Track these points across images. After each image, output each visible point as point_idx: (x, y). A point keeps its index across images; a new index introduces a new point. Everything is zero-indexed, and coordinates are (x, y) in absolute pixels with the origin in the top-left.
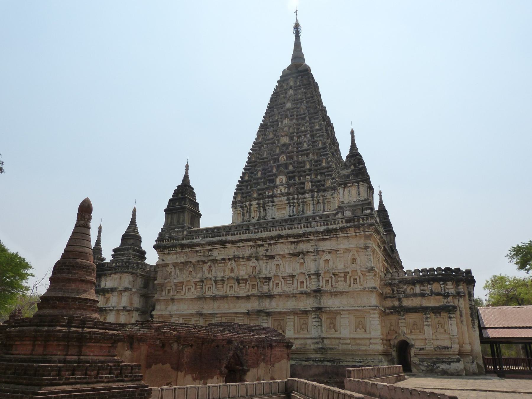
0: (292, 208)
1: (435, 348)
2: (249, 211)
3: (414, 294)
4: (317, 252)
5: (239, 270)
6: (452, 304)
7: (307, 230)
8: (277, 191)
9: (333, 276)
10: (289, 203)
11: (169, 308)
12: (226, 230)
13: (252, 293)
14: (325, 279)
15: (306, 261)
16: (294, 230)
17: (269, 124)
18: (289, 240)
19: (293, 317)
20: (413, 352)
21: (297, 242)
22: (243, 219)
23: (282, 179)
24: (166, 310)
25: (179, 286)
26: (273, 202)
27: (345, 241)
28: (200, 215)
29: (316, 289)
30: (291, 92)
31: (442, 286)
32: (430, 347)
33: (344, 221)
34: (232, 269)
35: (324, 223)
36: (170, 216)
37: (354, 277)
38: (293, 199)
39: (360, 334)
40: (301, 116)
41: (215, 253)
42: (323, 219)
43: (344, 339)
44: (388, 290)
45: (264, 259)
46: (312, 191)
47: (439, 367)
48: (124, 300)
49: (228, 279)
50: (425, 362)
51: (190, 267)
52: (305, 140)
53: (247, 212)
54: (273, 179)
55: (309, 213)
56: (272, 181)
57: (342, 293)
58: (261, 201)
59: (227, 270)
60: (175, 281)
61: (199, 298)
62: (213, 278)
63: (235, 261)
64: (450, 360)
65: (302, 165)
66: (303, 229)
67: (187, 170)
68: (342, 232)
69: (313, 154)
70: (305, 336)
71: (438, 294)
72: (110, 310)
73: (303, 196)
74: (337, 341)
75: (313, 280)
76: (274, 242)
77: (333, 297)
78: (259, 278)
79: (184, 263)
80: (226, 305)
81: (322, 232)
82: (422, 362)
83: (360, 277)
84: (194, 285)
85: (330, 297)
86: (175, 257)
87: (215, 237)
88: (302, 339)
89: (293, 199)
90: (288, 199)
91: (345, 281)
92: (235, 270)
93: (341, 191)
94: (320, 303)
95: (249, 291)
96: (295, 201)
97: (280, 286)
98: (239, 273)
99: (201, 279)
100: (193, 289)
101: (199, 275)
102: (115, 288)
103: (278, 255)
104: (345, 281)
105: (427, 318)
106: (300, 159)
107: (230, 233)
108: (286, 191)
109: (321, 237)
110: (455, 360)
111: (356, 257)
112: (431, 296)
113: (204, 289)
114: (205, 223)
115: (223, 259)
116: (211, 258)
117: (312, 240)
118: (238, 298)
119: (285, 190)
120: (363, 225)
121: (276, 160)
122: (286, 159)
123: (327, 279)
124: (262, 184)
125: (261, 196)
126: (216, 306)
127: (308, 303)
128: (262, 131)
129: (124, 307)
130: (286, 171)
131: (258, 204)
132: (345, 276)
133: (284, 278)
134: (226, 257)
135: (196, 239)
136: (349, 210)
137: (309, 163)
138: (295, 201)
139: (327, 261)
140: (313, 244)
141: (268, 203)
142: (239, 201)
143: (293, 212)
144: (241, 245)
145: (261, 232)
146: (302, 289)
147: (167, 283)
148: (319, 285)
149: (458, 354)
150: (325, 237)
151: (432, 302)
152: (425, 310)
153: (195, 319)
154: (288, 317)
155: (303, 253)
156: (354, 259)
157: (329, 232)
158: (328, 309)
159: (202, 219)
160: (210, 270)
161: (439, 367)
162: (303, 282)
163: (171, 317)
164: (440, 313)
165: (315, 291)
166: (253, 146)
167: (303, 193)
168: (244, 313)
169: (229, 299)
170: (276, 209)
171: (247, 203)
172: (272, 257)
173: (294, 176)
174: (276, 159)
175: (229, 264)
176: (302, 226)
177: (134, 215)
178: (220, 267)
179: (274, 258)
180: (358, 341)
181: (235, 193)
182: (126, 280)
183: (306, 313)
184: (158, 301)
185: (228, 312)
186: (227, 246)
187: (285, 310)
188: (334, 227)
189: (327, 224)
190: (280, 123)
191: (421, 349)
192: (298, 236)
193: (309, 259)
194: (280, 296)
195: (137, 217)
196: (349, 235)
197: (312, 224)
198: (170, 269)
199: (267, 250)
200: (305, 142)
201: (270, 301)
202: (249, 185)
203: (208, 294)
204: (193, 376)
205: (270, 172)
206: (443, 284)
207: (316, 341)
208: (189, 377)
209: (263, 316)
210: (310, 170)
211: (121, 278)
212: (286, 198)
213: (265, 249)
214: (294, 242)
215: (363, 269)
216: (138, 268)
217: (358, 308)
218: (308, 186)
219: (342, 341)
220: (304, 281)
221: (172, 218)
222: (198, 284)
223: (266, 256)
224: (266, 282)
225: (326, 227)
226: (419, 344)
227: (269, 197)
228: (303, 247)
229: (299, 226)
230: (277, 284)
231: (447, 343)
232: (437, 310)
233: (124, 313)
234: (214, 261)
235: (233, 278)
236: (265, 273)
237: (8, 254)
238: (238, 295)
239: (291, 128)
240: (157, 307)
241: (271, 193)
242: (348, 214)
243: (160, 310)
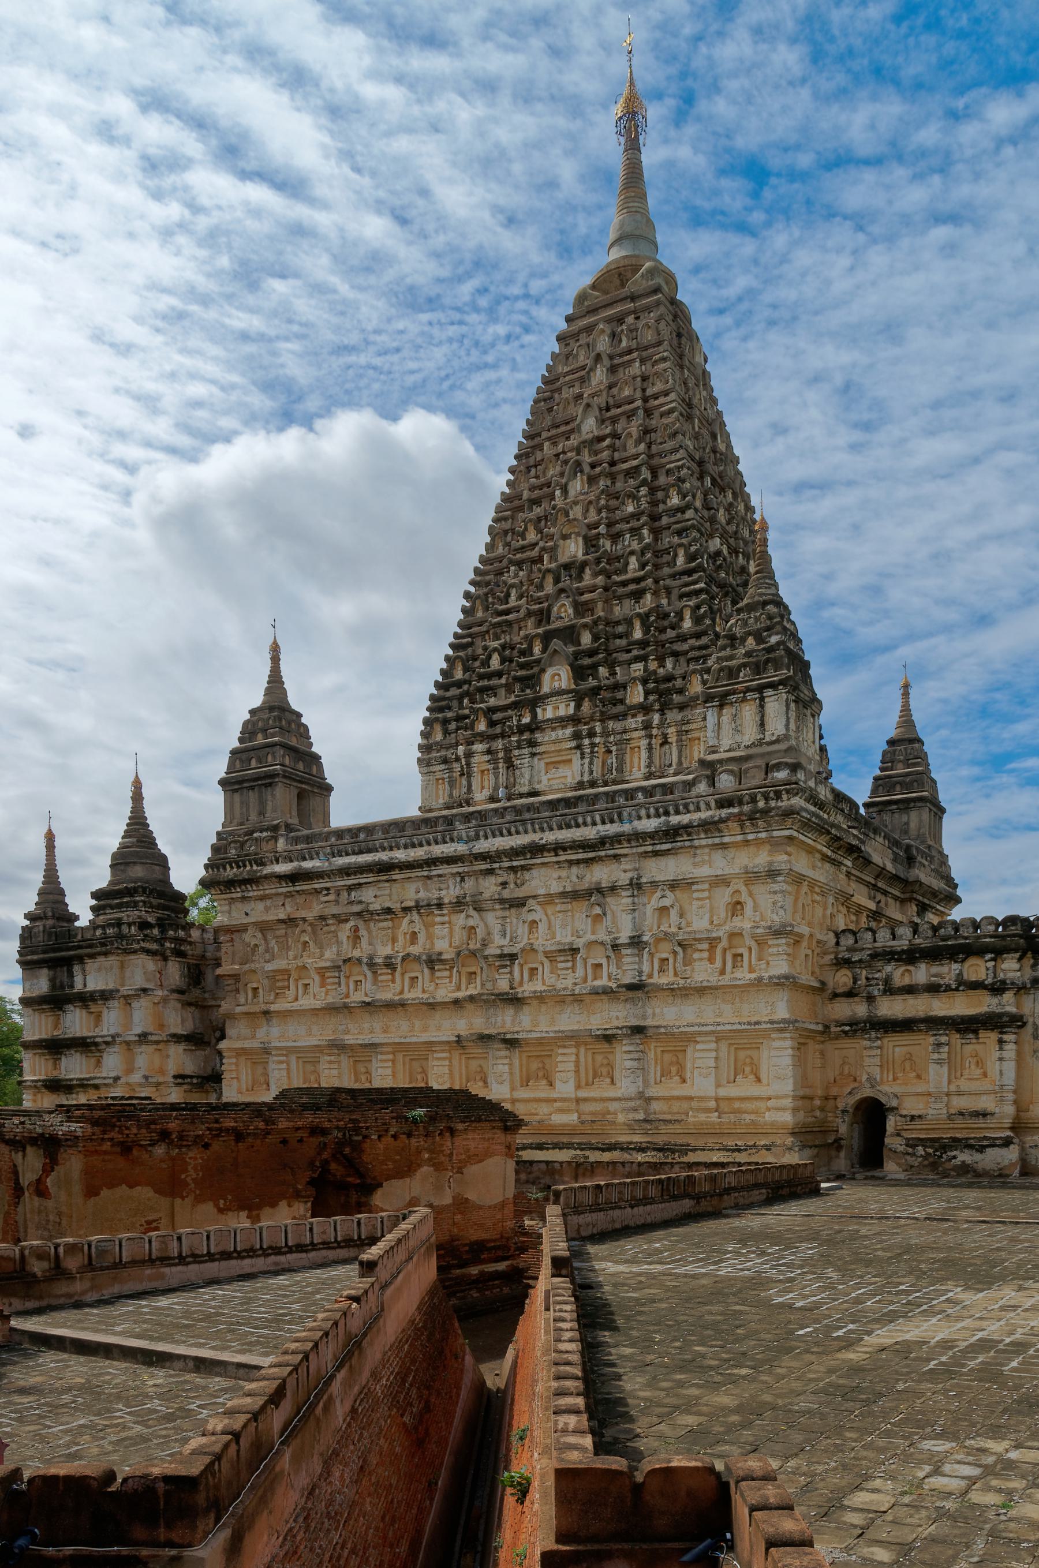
0: (587, 761)
1: (950, 1117)
2: (467, 773)
3: (910, 986)
4: (636, 885)
5: (430, 937)
6: (1012, 1009)
7: (611, 829)
8: (547, 712)
9: (679, 949)
10: (579, 747)
11: (261, 1033)
12: (396, 830)
13: (468, 993)
14: (658, 956)
15: (609, 912)
16: (574, 830)
17: (526, 495)
18: (562, 858)
19: (574, 1050)
20: (891, 1123)
21: (588, 862)
22: (451, 796)
23: (558, 677)
24: (254, 1037)
25: (279, 980)
26: (532, 743)
27: (717, 856)
28: (329, 789)
29: (633, 981)
30: (600, 376)
31: (991, 964)
32: (935, 1111)
33: (713, 804)
34: (414, 934)
35: (657, 810)
36: (237, 797)
37: (734, 951)
38: (591, 734)
39: (744, 1088)
40: (625, 466)
41: (367, 895)
42: (656, 799)
43: (701, 1099)
44: (843, 979)
45: (497, 907)
46: (645, 708)
47: (955, 1157)
48: (141, 1017)
49: (403, 959)
50: (920, 1148)
51: (304, 931)
52: (635, 546)
53: (462, 775)
54: (532, 676)
55: (636, 775)
56: (532, 681)
57: (701, 991)
58: (499, 744)
59: (401, 938)
60: (269, 967)
61: (332, 1009)
62: (365, 960)
63: (419, 913)
64: (985, 1143)
65: (620, 629)
66: (600, 827)
67: (275, 660)
68: (706, 832)
69: (656, 593)
70: (605, 1095)
71: (976, 985)
72: (107, 1043)
74: (685, 1105)
76: (522, 863)
78: (486, 957)
79: (290, 922)
80: (404, 1025)
81: (652, 835)
82: (914, 1146)
83: (750, 949)
84: (317, 978)
85: (670, 1000)
86: (260, 906)
87: (361, 852)
88: (595, 1100)
89: (591, 734)
90: (577, 736)
91: (711, 960)
92: (421, 937)
93: (711, 717)
94: (644, 1017)
95: (459, 989)
96: (597, 740)
97: (540, 977)
98: (433, 944)
99: (332, 961)
100: (315, 987)
101: (330, 954)
102: (111, 991)
103: (534, 897)
104: (711, 960)
105: (939, 1045)
106: (617, 610)
107: (403, 841)
108: (571, 711)
109: (650, 848)
110: (998, 1142)
111: (744, 897)
113: (343, 987)
114: (343, 812)
115: (388, 911)
117: (625, 855)
118: (432, 1006)
119: (566, 708)
120: (765, 812)
121: (543, 616)
122: (571, 611)
123: (664, 955)
124: (502, 692)
125: (498, 730)
126: (377, 1026)
127: (615, 1015)
128: (505, 519)
129: (139, 1036)
130: (571, 649)
131: (489, 752)
132: (712, 949)
133: (548, 955)
134: (396, 906)
135: (312, 858)
136: (731, 772)
137: (643, 624)
138: (597, 740)
139: (664, 910)
140: (628, 867)
141: (519, 748)
142: (437, 743)
143: (591, 772)
144: (434, 873)
145: (486, 838)
146: (598, 983)
147: (245, 973)
148: (640, 973)
149: (1012, 1129)
151: (961, 1006)
152: (934, 1023)
153: (328, 1058)
154: (560, 1051)
155: (599, 890)
156: (739, 903)
157: (671, 833)
158: (663, 1030)
159: (335, 800)
160: (356, 938)
161: (955, 1157)
162: (600, 965)
163: (269, 1053)
164: (976, 1032)
165: (632, 987)
166: (476, 571)
167: (623, 716)
168: (448, 1042)
169: (411, 1009)
170: (542, 764)
171: (461, 750)
172: (518, 903)
173: (594, 667)
174: (541, 611)
175: (406, 921)
176: (598, 818)
177: (137, 797)
178: (384, 929)
180: (737, 1105)
181: (426, 722)
182: (140, 970)
183: (608, 1038)
184: (230, 1016)
185: (408, 1040)
186: (396, 875)
187: (552, 1035)
188: (685, 819)
189: (667, 813)
190: (558, 493)
191: (913, 1118)
193: (619, 904)
194: (540, 998)
195: (146, 803)
196: (726, 840)
197: (625, 814)
198: (251, 937)
199: (504, 884)
200: (632, 553)
201: (516, 1013)
202: (467, 694)
203: (357, 997)
204: (217, 1206)
205: (523, 653)
206: (992, 959)
207: (632, 1104)
208: (209, 1207)
209: (499, 1049)
210: (643, 644)
211: (122, 966)
212: (569, 731)
213: (500, 880)
214: (578, 862)
215: (760, 931)
216: (165, 939)
217: (739, 1027)
218: (636, 695)
219: (694, 1104)
220: (604, 961)
221: (245, 804)
222: (327, 975)
223: (502, 901)
224: (505, 966)
225: (663, 818)
226: (911, 1106)
227: (522, 729)
228: (601, 874)
229: (589, 819)
230: (533, 971)
231: (986, 1103)
232: (968, 1026)
234: (366, 915)
235: (417, 959)
236: (498, 944)
238: (431, 1000)
239: (592, 510)
240: (230, 1032)
241: (526, 720)
242: (726, 782)
243: (238, 1038)
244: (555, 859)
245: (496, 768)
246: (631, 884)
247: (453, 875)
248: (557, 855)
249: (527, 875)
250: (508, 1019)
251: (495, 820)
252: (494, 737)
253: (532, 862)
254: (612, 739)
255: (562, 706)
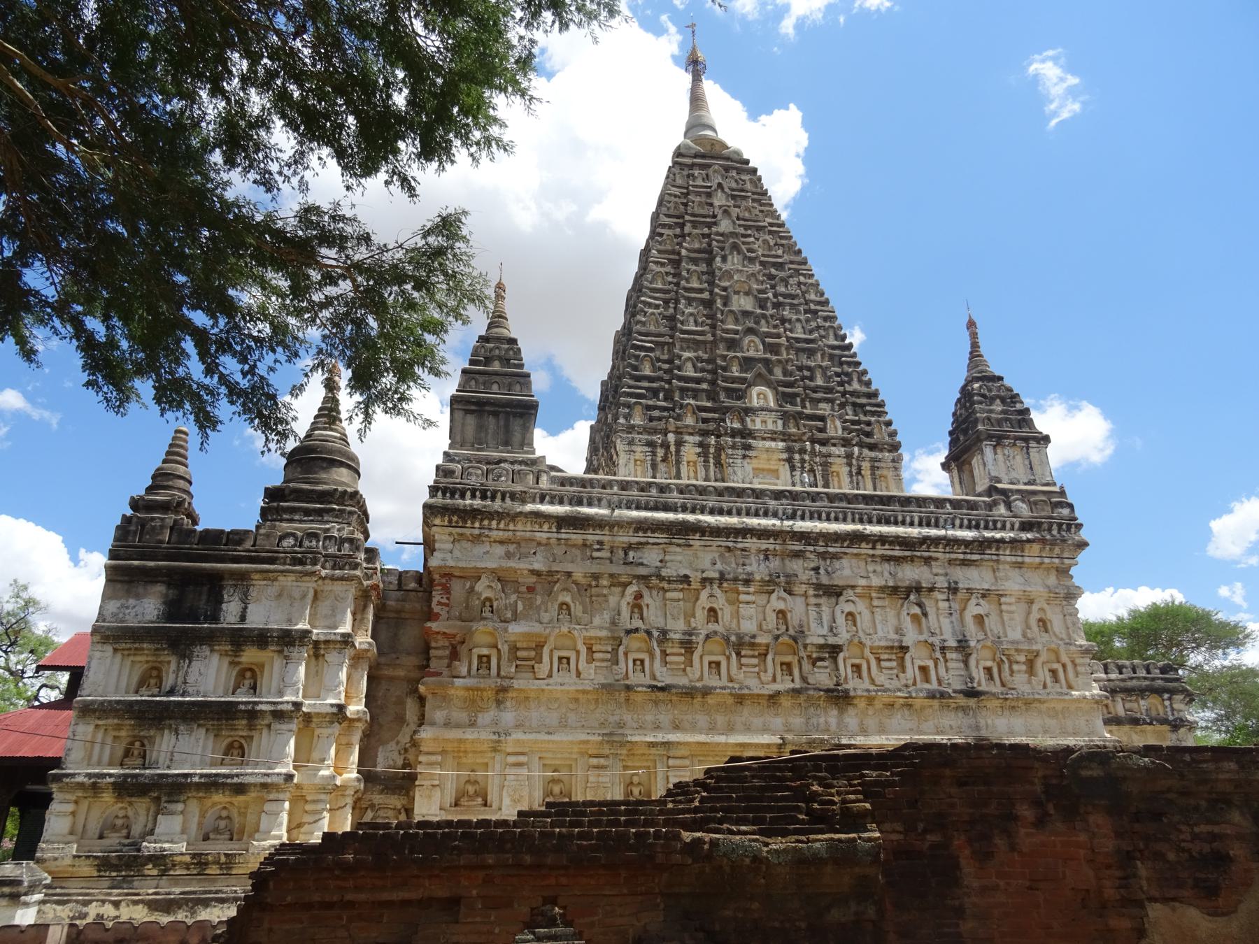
4: (953, 589)
5: (737, 615)
8: (756, 423)
21: (897, 560)
23: (761, 396)
26: (748, 447)
35: (970, 521)
41: (651, 557)
73: (824, 450)
75: (950, 664)
77: (1007, 713)
86: (499, 550)
89: (802, 451)
90: (789, 450)
103: (853, 587)
109: (961, 556)
112: (1151, 724)
115: (685, 579)
116: (642, 571)
132: (1031, 664)
141: (733, 447)
150: (969, 557)
155: (918, 589)
157: (983, 545)
160: (637, 607)
170: (749, 468)
172: (834, 592)
179: (839, 595)
192: (905, 542)
213: (812, 565)
220: (930, 664)
227: (734, 433)
228: (910, 574)
229: (908, 519)
233: (336, 729)
236: (816, 635)
237: (1114, 423)
241: (736, 425)
244: (871, 552)
245: (706, 461)
246: (949, 588)
247: (759, 551)
248: (874, 548)
249: (837, 564)
250: (833, 721)
251: (808, 502)
252: (705, 433)
253: (848, 550)
254: (818, 459)
255: (770, 422)
